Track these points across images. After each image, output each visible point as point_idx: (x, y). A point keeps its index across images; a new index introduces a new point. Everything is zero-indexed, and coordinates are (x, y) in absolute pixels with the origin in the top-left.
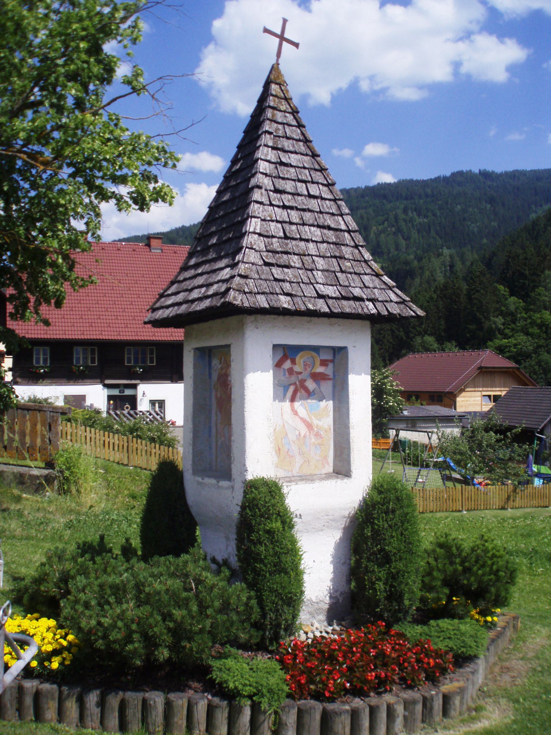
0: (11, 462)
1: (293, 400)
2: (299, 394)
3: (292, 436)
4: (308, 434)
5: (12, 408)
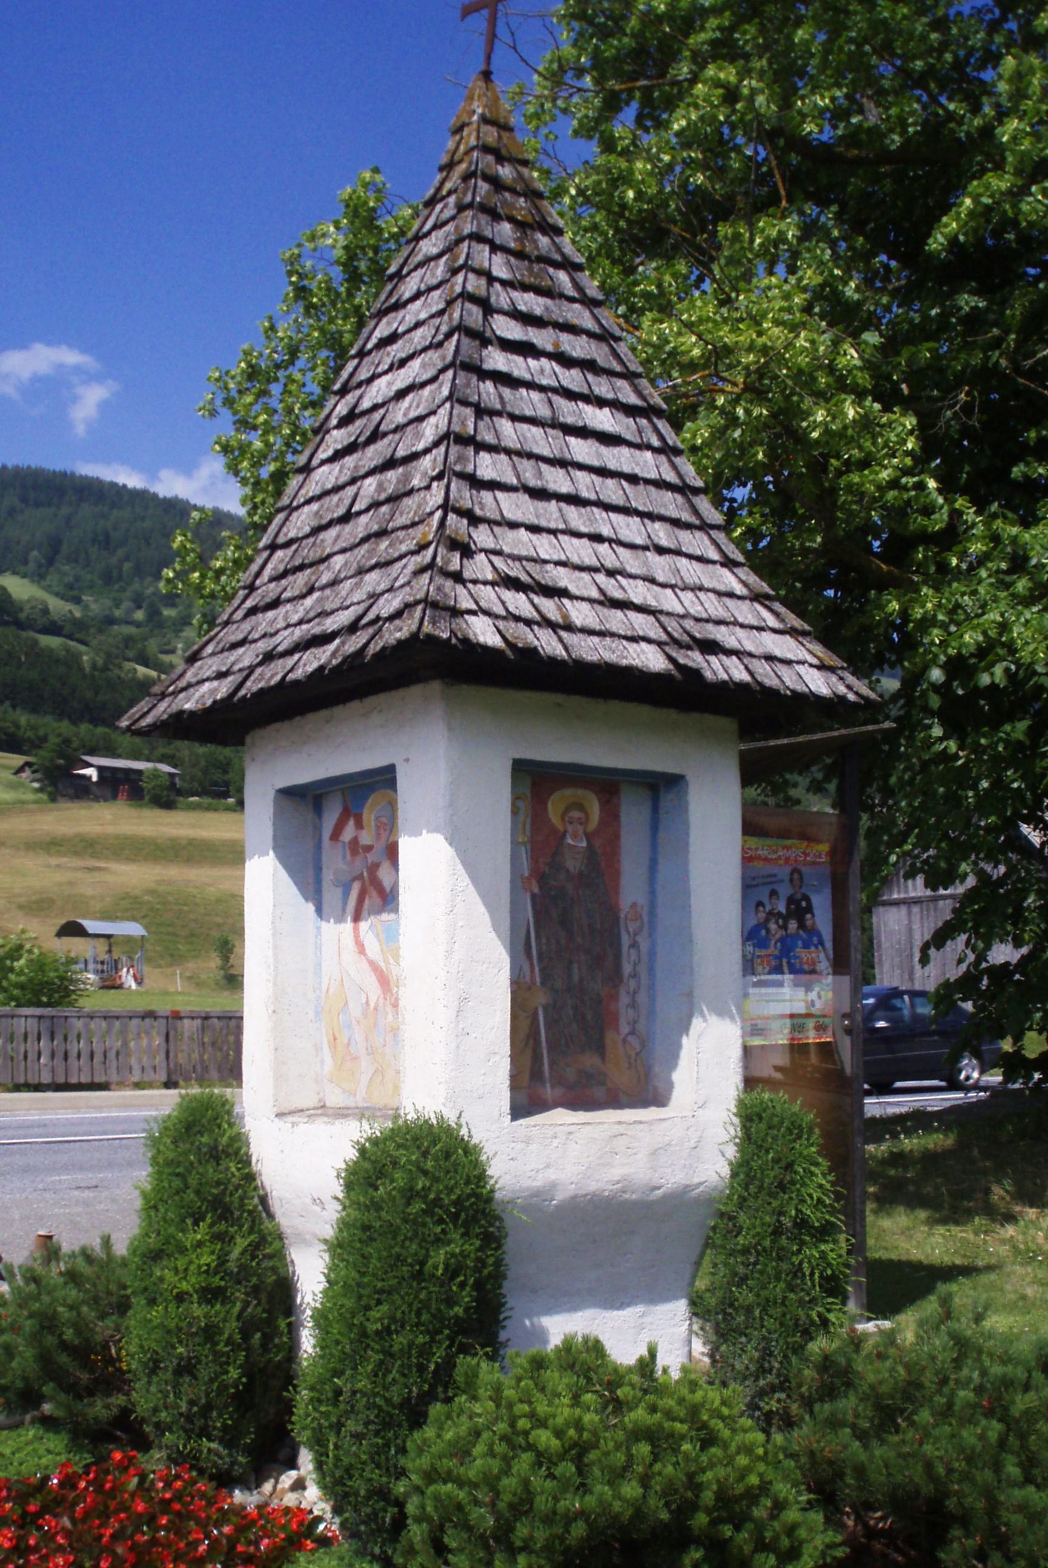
0: (405, 255)
1: (357, 918)
2: (367, 902)
3: (355, 1009)
4: (381, 1001)
5: (14, 1522)
